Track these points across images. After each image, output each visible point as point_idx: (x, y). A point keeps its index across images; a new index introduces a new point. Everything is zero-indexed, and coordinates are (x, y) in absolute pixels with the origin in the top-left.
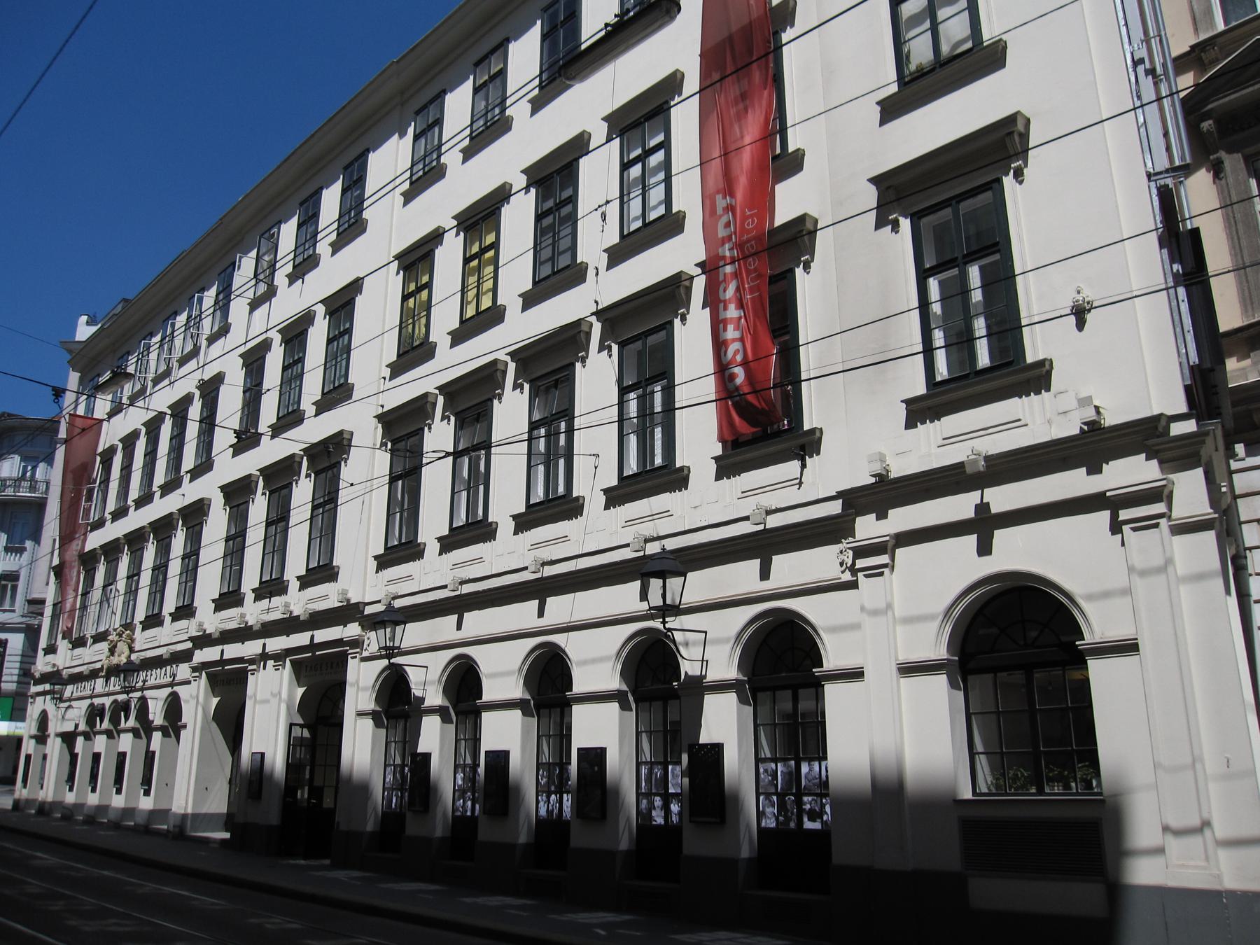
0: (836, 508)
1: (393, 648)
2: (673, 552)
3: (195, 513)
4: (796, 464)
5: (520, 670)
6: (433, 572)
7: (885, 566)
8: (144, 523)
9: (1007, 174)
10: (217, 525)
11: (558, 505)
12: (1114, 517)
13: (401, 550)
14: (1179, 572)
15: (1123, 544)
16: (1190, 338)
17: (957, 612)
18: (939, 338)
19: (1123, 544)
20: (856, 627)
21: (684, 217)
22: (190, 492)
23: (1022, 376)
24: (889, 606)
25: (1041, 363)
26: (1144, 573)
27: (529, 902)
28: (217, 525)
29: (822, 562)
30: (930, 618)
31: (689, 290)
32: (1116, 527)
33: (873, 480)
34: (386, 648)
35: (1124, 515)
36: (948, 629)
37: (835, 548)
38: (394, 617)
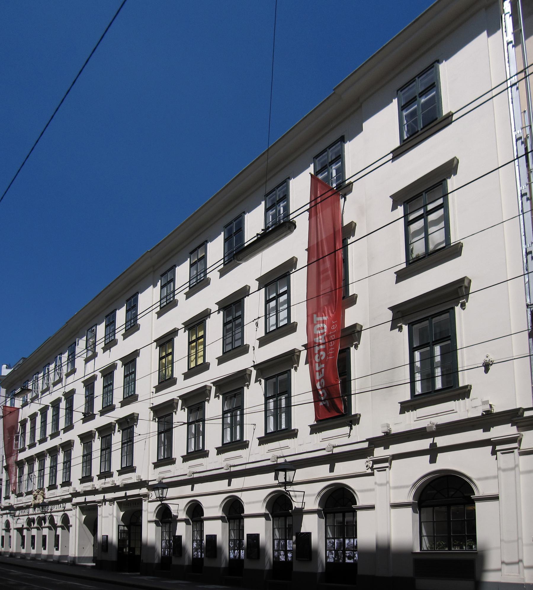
0: (366, 445)
1: (163, 497)
3: (68, 446)
5: (265, 500)
6: (180, 469)
7: (387, 467)
8: (113, 420)
9: (457, 305)
10: (78, 450)
13: (86, 478)
15: (496, 459)
17: (418, 485)
19: (496, 459)
20: (372, 490)
22: (64, 438)
23: (456, 391)
24: (388, 482)
25: (466, 387)
28: (78, 450)
29: (359, 465)
30: (407, 487)
31: (299, 357)
32: (494, 452)
34: (159, 497)
35: (498, 448)
36: (221, 510)
37: (364, 460)
38: (162, 486)
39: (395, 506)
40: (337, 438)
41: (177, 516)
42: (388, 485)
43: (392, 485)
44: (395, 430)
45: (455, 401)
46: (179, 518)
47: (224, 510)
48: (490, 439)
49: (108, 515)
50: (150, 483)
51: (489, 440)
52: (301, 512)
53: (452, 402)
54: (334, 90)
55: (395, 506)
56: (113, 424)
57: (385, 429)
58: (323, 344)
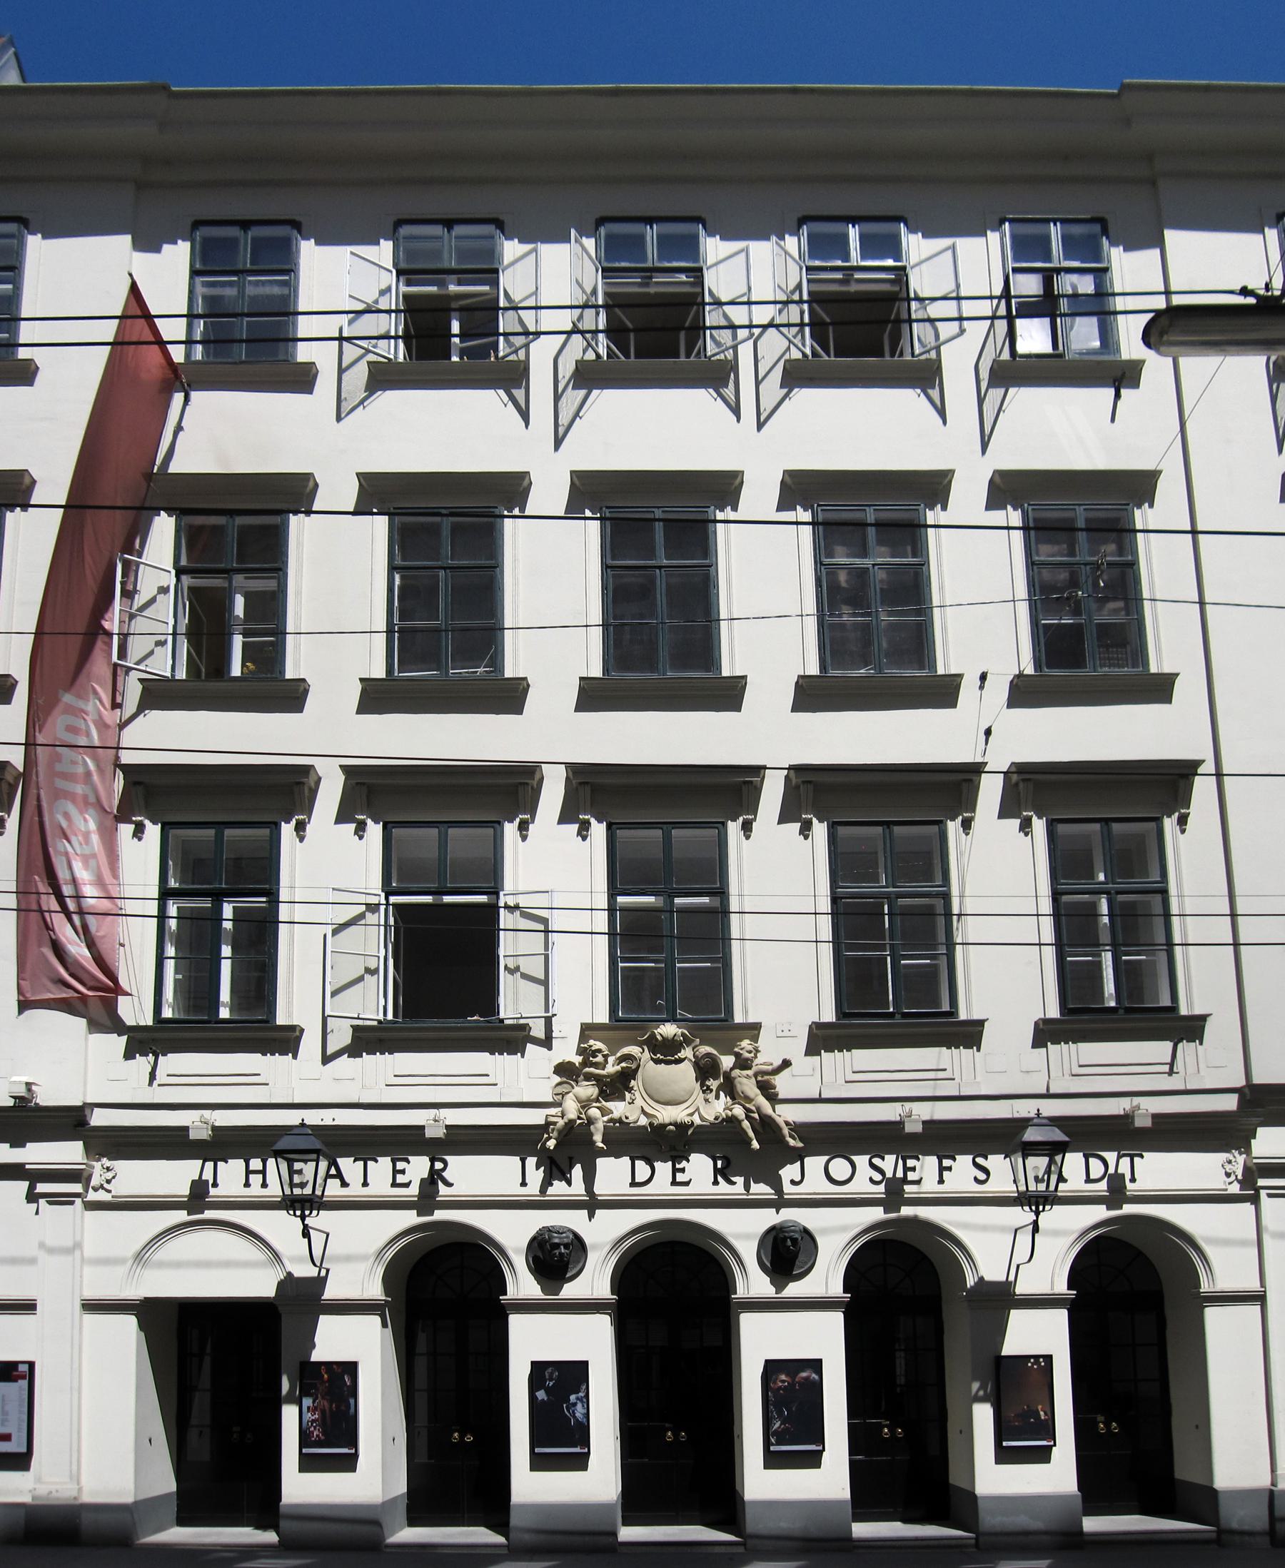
2: (315, 1128)
4: (1168, 1045)
7: (77, 1195)
11: (257, 1029)
12: (32, 1188)
14: (86, 1254)
15: (37, 1213)
16: (515, 1022)
18: (170, 951)
19: (37, 1213)
20: (32, 1261)
21: (306, 692)
23: (1154, 1016)
24: (78, 1246)
25: (292, 1028)
26: (51, 1251)
27: (308, 1561)
29: (1205, 1169)
30: (364, 1258)
31: (757, 791)
32: (32, 1197)
33: (11, 1103)
35: (42, 1188)
36: (380, 1271)
37: (1222, 1157)
39: (94, 1306)
40: (1119, 1071)
41: (320, 1282)
42: (77, 1253)
43: (89, 1251)
44: (47, 1097)
45: (492, 1053)
46: (332, 1292)
47: (389, 1280)
48: (24, 1165)
49: (33, 1251)
50: (99, 1119)
51: (22, 1165)
52: (1000, 1299)
53: (257, 1056)
54: (1124, 88)
55: (94, 1306)
56: (9, 777)
57: (22, 1091)
58: (71, 797)
